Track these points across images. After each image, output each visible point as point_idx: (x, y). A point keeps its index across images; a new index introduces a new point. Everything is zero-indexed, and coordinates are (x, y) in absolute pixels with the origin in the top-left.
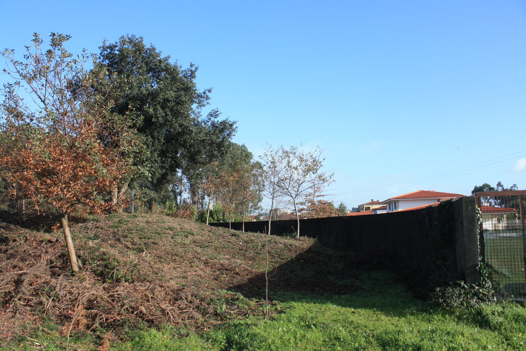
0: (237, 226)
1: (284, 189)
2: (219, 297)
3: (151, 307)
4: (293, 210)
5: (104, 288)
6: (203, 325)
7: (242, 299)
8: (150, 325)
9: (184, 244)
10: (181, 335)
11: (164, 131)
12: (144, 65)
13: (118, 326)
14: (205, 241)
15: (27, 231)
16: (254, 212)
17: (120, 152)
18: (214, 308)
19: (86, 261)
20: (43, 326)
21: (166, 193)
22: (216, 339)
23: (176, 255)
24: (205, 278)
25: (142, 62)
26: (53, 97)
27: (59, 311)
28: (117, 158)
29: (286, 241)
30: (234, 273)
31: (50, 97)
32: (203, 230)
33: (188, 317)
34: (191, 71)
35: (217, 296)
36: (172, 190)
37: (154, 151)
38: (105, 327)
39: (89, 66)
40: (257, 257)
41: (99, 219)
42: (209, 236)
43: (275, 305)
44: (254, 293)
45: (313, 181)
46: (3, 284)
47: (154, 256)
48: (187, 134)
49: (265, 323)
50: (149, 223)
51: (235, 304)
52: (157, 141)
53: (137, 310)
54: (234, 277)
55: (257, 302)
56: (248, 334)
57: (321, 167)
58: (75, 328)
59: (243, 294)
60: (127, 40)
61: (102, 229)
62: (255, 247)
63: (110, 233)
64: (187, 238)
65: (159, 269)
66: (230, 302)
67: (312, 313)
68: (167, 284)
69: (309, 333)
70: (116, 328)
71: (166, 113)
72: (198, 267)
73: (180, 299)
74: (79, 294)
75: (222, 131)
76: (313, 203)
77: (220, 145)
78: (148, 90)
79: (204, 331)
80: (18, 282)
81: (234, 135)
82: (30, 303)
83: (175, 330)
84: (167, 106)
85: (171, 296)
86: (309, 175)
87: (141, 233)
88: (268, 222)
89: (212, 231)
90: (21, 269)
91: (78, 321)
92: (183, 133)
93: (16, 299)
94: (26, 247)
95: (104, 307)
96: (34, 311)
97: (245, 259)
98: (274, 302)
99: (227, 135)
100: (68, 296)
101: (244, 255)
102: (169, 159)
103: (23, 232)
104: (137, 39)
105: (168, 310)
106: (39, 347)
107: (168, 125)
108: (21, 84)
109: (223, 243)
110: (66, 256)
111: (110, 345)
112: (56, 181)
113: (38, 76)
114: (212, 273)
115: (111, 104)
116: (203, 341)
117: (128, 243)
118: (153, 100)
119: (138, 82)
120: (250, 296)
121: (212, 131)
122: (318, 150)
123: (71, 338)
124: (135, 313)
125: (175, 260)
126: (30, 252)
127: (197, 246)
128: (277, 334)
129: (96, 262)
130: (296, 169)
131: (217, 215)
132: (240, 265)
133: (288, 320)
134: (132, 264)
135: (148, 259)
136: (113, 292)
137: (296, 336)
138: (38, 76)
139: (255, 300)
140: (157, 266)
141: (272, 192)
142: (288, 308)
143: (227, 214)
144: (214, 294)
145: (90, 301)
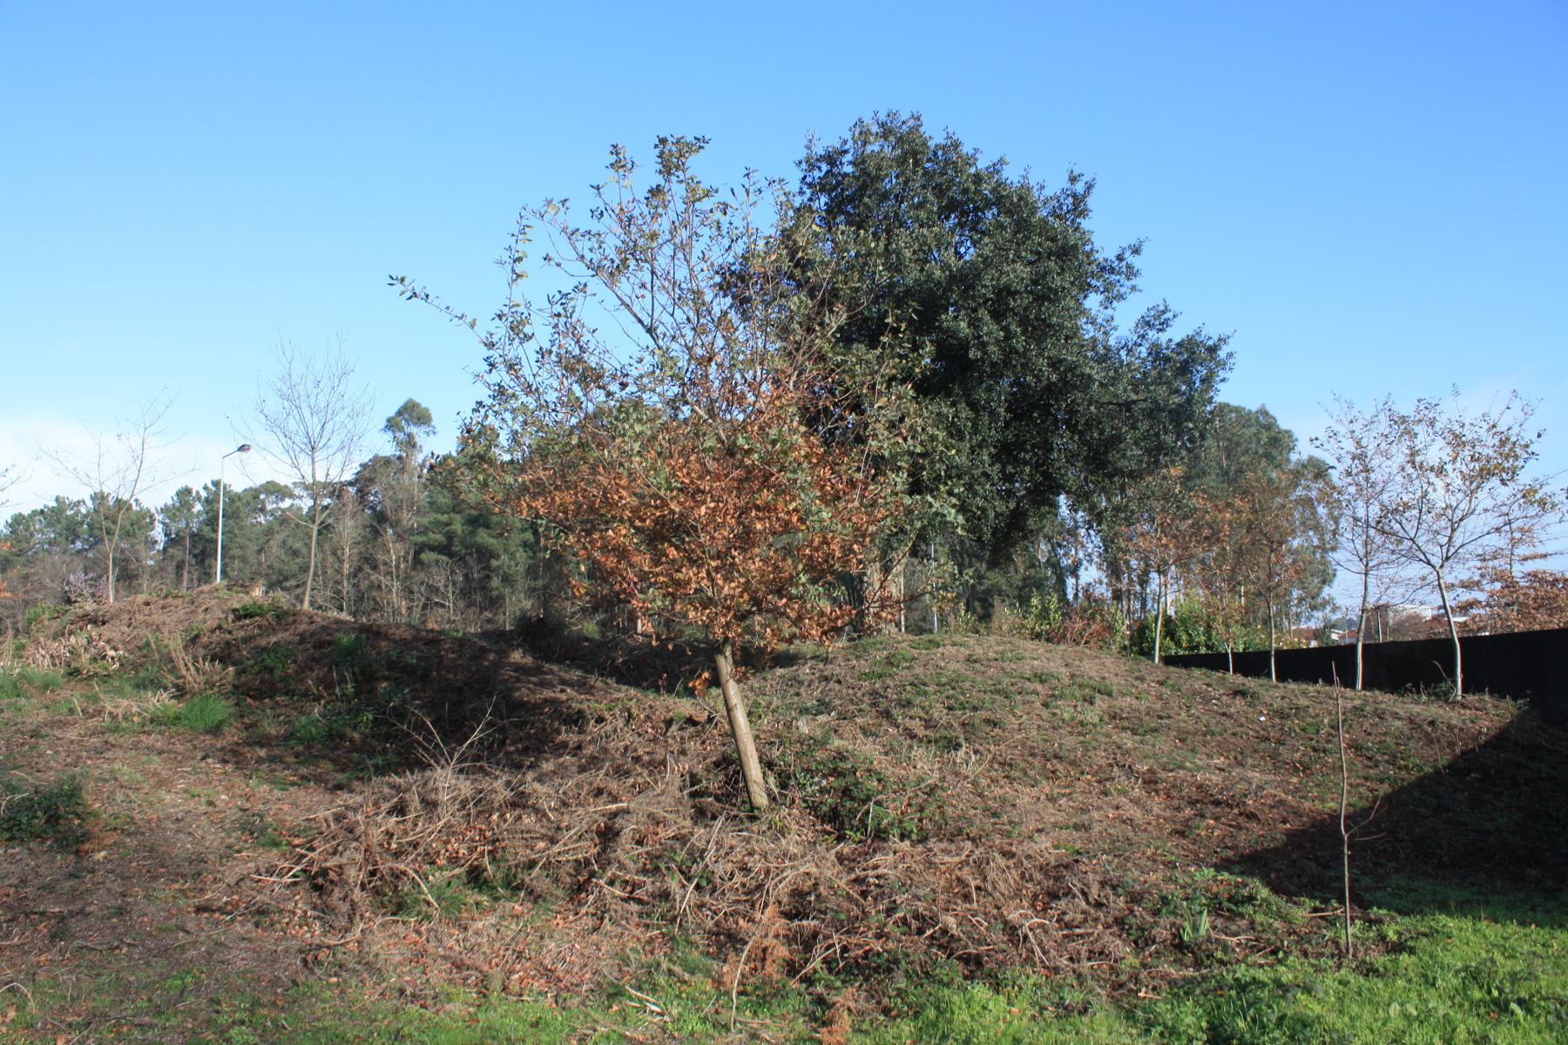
0: (1252, 663)
1: (1400, 541)
2: (1189, 891)
3: (973, 916)
4: (1439, 608)
5: (840, 858)
6: (1135, 978)
7: (1264, 900)
8: (971, 972)
9: (1082, 723)
10: (1066, 1008)
11: (1005, 383)
12: (930, 197)
13: (876, 970)
14: (1148, 714)
15: (632, 691)
16: (1309, 619)
17: (868, 455)
18: (1173, 925)
19: (789, 777)
20: (670, 960)
21: (1032, 571)
22: (1174, 1027)
23: (1056, 757)
24: (1145, 830)
25: (924, 187)
26: (672, 315)
27: (712, 918)
28: (860, 476)
29: (1416, 709)
30: (1241, 814)
31: (666, 318)
32: (1142, 679)
33: (1090, 951)
34: (1074, 196)
35: (1183, 887)
36: (1048, 561)
37: (980, 445)
38: (838, 973)
39: (766, 220)
40: (1316, 762)
41: (831, 656)
42: (1160, 698)
43: (1379, 921)
44: (1305, 880)
45: (1505, 510)
46: (571, 838)
47: (991, 762)
48: (1075, 387)
49: (1340, 982)
50: (975, 661)
51: (1242, 916)
52: (986, 419)
53: (934, 926)
54: (1238, 827)
55: (1315, 910)
56: (1281, 1019)
57: (1532, 462)
58: (755, 969)
59: (1268, 884)
60: (875, 129)
61: (839, 682)
62: (1311, 730)
63: (863, 695)
64: (1092, 703)
65: (1003, 800)
66: (1226, 908)
67: (1512, 957)
68: (1029, 848)
69: (1503, 1029)
70: (870, 975)
71: (1006, 329)
72: (1124, 793)
73: (1065, 895)
74: (768, 872)
75: (1184, 370)
76: (1510, 585)
77: (1181, 415)
78: (948, 267)
79: (1138, 998)
80: (608, 835)
81: (1223, 380)
82: (638, 893)
83: (1046, 991)
84: (1008, 309)
85: (1039, 883)
86: (1486, 490)
87: (951, 692)
88: (1353, 647)
89: (1171, 682)
90: (615, 799)
91: (765, 950)
92: (1064, 387)
93: (602, 882)
94: (629, 738)
95: (837, 912)
96: (648, 915)
97: (1276, 768)
98: (1375, 912)
99: (1202, 381)
100: (739, 878)
101: (1274, 756)
102: (1027, 469)
103: (622, 695)
104: (904, 123)
105: (1025, 929)
106: (659, 1018)
107: (1015, 366)
108: (589, 290)
109: (1204, 719)
110: (734, 762)
111: (852, 1027)
112: (693, 551)
113: (632, 263)
114: (1168, 813)
115: (837, 319)
116: (1134, 1031)
117: (913, 722)
118: (964, 294)
119: (916, 247)
120: (1293, 888)
121: (1153, 373)
122: (1517, 405)
123: (744, 998)
124: (928, 933)
125: (1053, 772)
126: (640, 752)
127: (1124, 729)
128: (1384, 1024)
129: (816, 779)
130: (1440, 471)
132: (1260, 788)
133: (1425, 976)
134: (923, 785)
135: (970, 770)
136: (864, 870)
137: (1451, 1039)
138: (632, 263)
139: (1309, 903)
140: (998, 791)
141: (1362, 552)
142: (1425, 935)
143: (1218, 626)
144: (1176, 882)
145: (798, 894)
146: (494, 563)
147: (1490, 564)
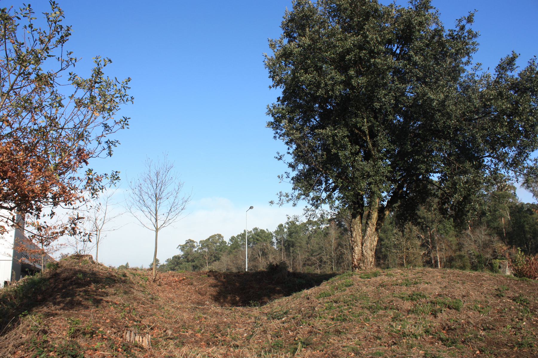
146: (383, 243)
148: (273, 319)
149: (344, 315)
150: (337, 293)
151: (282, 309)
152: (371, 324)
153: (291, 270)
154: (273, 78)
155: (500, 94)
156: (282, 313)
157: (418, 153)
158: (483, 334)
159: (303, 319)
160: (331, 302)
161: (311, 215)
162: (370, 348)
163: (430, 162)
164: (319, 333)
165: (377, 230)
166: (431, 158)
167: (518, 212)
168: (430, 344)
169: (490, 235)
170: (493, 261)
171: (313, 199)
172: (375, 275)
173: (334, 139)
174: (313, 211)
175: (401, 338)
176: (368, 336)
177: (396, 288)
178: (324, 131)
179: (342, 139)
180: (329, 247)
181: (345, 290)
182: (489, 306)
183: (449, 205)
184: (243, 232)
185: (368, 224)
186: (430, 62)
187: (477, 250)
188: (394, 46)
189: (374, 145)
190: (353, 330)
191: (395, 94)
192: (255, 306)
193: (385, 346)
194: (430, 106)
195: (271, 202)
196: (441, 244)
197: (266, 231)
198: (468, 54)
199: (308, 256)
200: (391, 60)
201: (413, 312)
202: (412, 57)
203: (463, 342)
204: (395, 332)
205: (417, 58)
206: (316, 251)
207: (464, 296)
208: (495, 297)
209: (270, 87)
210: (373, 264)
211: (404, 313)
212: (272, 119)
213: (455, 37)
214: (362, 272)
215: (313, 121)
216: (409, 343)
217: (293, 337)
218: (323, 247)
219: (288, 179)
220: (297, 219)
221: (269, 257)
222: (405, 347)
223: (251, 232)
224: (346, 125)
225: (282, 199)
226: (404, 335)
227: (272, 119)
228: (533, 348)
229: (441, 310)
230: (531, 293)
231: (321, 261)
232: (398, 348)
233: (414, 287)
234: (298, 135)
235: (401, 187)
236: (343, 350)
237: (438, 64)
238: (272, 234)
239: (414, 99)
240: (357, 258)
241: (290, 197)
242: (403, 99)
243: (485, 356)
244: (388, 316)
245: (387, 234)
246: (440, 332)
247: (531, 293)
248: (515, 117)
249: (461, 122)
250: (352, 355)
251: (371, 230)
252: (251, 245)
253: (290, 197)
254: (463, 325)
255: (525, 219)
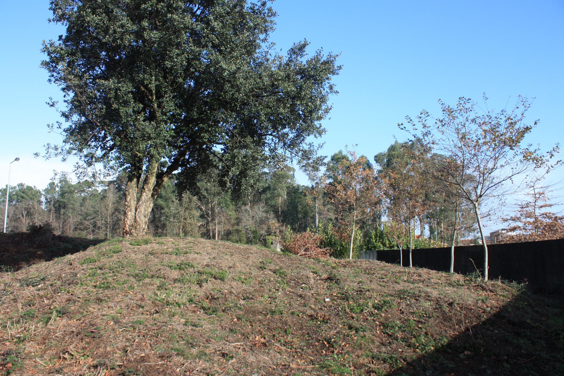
131: (389, 240)
146: (163, 211)
147: (525, 209)
148: (28, 286)
149: (107, 282)
150: (104, 260)
151: (40, 275)
152: (135, 292)
153: (57, 233)
154: (54, 10)
155: (288, 76)
156: (38, 279)
157: (203, 121)
158: (242, 303)
159: (62, 286)
160: (96, 268)
161: (81, 173)
162: (131, 316)
163: (214, 132)
164: (79, 301)
165: (153, 195)
166: (215, 128)
167: (294, 193)
168: (192, 313)
169: (267, 212)
170: (267, 237)
171: (86, 156)
172: (146, 242)
173: (116, 92)
174: (85, 168)
175: (164, 306)
176: (130, 304)
177: (166, 256)
178: (106, 83)
179: (126, 95)
180: (105, 212)
181: (112, 257)
182: (251, 278)
183: (228, 178)
184: (5, 187)
185: (144, 189)
186: (229, 30)
187: (254, 225)
188: (195, 6)
189: (159, 106)
190: (116, 298)
191: (188, 56)
192: (7, 271)
193: (147, 314)
194: (221, 76)
195: (36, 154)
196: (220, 217)
197: (34, 188)
198: (266, 31)
199: (81, 219)
200: (188, 20)
201: (179, 281)
202: (211, 22)
203: (223, 311)
204: (159, 301)
205: (216, 24)
206: (90, 215)
207: (230, 267)
208: (258, 269)
209: (50, 21)
210: (145, 231)
211: (170, 282)
212: (47, 59)
213: (256, 11)
214: (132, 238)
215: (97, 69)
216: (171, 312)
217: (48, 306)
218: (98, 211)
219: (59, 129)
220: (65, 175)
221: (35, 218)
222: (167, 315)
223: (15, 187)
224: (132, 80)
225: (49, 152)
226: (168, 303)
227: (47, 59)
228: (283, 315)
229: (207, 280)
230: (290, 266)
231: (95, 226)
232: (160, 316)
233: (183, 256)
234: (76, 82)
235: (182, 154)
236: (102, 319)
237: (236, 34)
238: (40, 192)
239: (207, 66)
240: (129, 224)
241: (60, 150)
242: (195, 64)
243: (241, 323)
244: (153, 284)
245: (168, 202)
246: (204, 301)
247: (290, 266)
248: (297, 101)
249: (249, 97)
250: (111, 324)
251: (147, 195)
252: (14, 202)
253: (60, 150)
254: (226, 295)
255: (299, 200)
